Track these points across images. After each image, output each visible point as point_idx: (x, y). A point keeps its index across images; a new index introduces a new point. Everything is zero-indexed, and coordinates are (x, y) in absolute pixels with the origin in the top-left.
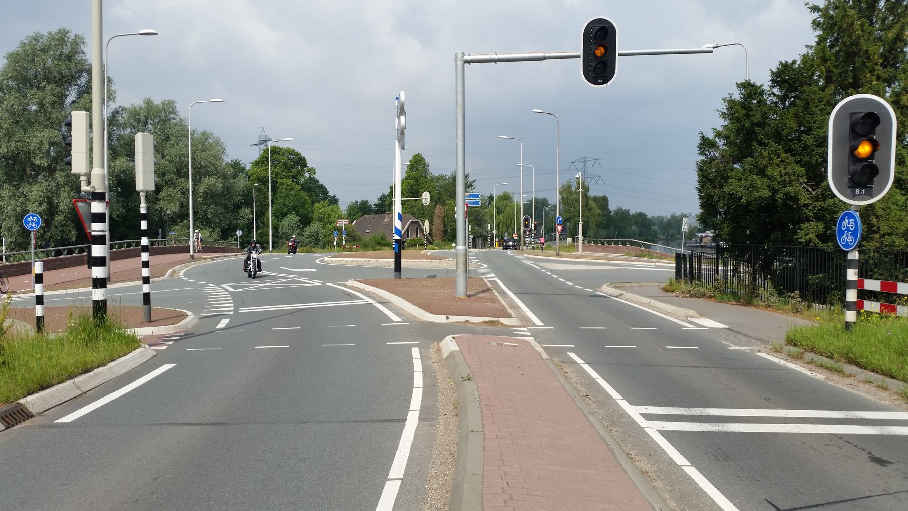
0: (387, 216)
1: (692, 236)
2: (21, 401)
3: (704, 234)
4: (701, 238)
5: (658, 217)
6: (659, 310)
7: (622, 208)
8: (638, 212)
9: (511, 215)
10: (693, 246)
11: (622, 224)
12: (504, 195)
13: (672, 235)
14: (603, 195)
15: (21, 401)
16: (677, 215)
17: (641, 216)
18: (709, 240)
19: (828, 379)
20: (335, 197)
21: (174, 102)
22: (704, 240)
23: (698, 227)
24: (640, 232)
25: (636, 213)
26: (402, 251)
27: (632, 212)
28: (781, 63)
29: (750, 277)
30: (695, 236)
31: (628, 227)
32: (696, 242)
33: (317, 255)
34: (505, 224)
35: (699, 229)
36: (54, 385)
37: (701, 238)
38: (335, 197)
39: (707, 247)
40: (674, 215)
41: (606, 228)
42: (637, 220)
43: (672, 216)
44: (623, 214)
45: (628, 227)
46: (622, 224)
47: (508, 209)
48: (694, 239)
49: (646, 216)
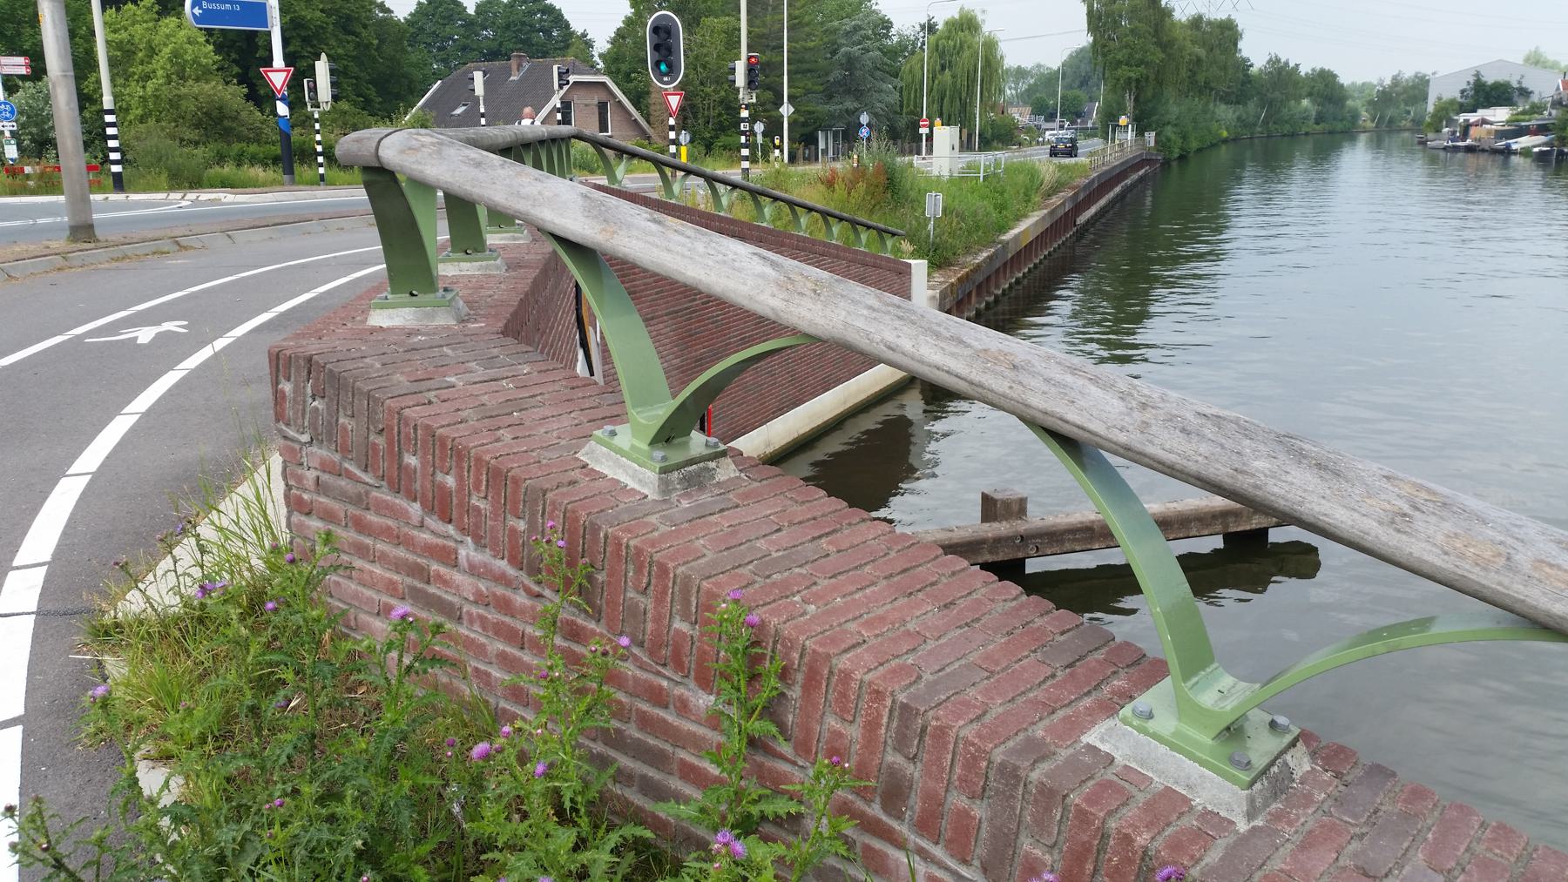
0: (514, 67)
1: (1441, 121)
3: (1473, 118)
4: (1466, 128)
6: (1178, 474)
7: (1280, 56)
8: (1318, 68)
10: (1445, 149)
11: (1277, 94)
12: (961, 18)
13: (1391, 121)
18: (1489, 132)
20: (584, 35)
21: (1417, 73)
22: (1473, 131)
23: (1459, 100)
24: (1319, 113)
25: (1313, 70)
27: (1304, 70)
29: (1199, 220)
30: (1450, 122)
33: (18, 223)
34: (957, 95)
35: (1461, 105)
36: (1530, 620)
37: (1466, 128)
38: (584, 35)
39: (1483, 151)
40: (1399, 75)
41: (1238, 103)
43: (1395, 78)
46: (1277, 94)
47: (966, 54)
48: (1446, 130)
49: (1335, 76)
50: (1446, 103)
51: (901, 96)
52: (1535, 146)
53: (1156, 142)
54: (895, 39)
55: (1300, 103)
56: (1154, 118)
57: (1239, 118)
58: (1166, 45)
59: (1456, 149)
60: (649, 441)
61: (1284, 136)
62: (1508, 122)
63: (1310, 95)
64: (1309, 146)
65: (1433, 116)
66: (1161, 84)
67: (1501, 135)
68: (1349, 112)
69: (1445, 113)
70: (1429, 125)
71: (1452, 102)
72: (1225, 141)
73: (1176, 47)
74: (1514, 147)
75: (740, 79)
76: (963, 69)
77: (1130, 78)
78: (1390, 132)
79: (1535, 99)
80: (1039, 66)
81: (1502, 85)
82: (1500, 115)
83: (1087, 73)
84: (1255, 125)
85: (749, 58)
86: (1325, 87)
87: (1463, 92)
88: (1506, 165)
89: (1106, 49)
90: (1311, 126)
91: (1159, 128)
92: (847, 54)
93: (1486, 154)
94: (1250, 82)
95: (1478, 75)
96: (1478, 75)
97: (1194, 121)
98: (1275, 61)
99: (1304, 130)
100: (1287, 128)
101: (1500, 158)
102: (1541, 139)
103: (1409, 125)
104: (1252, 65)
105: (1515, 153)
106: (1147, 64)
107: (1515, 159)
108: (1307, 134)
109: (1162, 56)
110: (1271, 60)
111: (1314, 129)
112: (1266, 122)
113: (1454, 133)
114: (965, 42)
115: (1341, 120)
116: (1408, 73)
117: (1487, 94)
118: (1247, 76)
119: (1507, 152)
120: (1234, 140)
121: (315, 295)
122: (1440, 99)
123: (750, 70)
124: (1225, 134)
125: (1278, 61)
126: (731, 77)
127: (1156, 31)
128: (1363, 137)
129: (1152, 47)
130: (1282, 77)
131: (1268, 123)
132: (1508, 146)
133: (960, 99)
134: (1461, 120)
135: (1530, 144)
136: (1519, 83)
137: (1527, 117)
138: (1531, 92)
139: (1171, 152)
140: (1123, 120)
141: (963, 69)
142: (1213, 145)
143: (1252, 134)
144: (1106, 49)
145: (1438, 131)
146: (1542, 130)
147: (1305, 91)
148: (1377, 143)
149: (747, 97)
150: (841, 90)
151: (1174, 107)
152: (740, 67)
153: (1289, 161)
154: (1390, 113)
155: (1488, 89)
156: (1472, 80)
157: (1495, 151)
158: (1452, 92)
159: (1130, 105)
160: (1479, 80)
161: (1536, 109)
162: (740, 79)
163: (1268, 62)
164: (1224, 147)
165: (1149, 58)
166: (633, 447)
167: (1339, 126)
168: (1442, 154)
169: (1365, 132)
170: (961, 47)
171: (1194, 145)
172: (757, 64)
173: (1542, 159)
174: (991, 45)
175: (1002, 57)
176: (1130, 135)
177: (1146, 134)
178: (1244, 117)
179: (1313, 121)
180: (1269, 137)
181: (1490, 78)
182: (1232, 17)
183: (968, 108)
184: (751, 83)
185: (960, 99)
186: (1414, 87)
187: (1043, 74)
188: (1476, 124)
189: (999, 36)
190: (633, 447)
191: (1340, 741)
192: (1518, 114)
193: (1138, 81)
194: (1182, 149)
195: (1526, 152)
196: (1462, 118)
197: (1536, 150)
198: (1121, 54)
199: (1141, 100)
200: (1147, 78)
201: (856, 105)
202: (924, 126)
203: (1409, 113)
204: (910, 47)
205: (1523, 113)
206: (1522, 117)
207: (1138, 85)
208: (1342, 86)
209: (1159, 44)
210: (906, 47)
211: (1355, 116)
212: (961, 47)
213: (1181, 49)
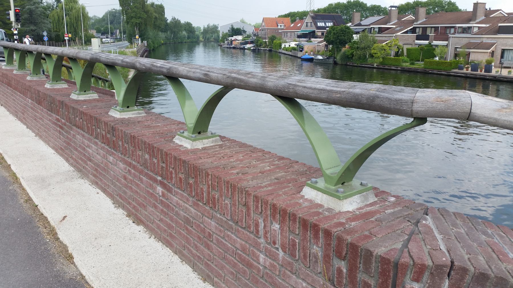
1: (224, 40)
2: (146, 115)
4: (232, 41)
5: (197, 27)
7: (175, 17)
8: (186, 22)
9: (77, 18)
13: (208, 39)
14: (160, 4)
15: (146, 115)
16: (211, 25)
17: (189, 25)
18: (238, 43)
19: (78, 97)
26: (300, 60)
28: (455, 2)
30: (227, 40)
31: (180, 32)
32: (228, 44)
40: (209, 25)
41: (165, 32)
42: (186, 28)
43: (208, 25)
44: (176, 22)
45: (180, 32)
46: (176, 29)
47: (74, 11)
48: (226, 42)
49: (191, 24)
50: (225, 34)
51: (53, 25)
52: (252, 47)
53: (147, 44)
54: (45, 4)
55: (182, 33)
56: (145, 36)
57: (166, 37)
58: (147, 12)
59: (230, 48)
60: (192, 133)
61: (179, 43)
62: (243, 40)
63: (185, 30)
64: (186, 46)
65: (222, 38)
66: (146, 25)
67: (242, 44)
68: (196, 36)
69: (225, 37)
70: (221, 40)
71: (227, 33)
72: (163, 44)
73: (150, 13)
74: (246, 47)
75: (12, 18)
76: (73, 16)
77: (136, 23)
78: (208, 42)
79: (248, 33)
80: (95, 16)
81: (239, 29)
82: (240, 38)
83: (112, 19)
84: (170, 39)
85: (15, 10)
86: (188, 27)
87: (229, 31)
88: (244, 54)
89: (127, 12)
90: (186, 40)
91: (147, 39)
92: (29, 9)
93: (238, 49)
94: (168, 25)
95: (232, 26)
96: (232, 26)
97: (155, 37)
98: (174, 19)
99: (185, 41)
100: (180, 40)
101: (242, 51)
102: (251, 45)
103: (213, 40)
104: (168, 20)
105: (246, 49)
106: (141, 18)
107: (246, 51)
108: (185, 42)
109: (146, 16)
110: (173, 18)
111: (187, 41)
112: (173, 38)
113: (228, 43)
114: (73, 7)
115: (195, 38)
116: (211, 24)
117: (235, 32)
118: (167, 23)
119: (244, 49)
120: (165, 44)
121: (61, 87)
122: (223, 33)
123: (17, 15)
124: (163, 42)
125: (175, 19)
126: (8, 17)
127: (143, 7)
128: (201, 44)
129: (143, 13)
130: (176, 23)
131: (174, 39)
132: (244, 47)
133: (74, 27)
134: (230, 39)
135: (250, 47)
136: (243, 28)
137: (247, 39)
138: (246, 31)
139: (151, 48)
140: (137, 37)
141: (73, 16)
142: (160, 45)
143: (170, 42)
144: (127, 12)
145: (224, 42)
146: (252, 42)
147: (183, 29)
148: (205, 46)
149: (16, 25)
150: (28, 22)
151: (151, 33)
152: (12, 13)
153: (181, 52)
154: (208, 36)
155: (235, 30)
156: (231, 27)
157: (241, 49)
158: (226, 31)
159: (137, 32)
160: (232, 27)
161: (249, 36)
162: (12, 18)
163: (172, 19)
164: (163, 46)
165: (142, 16)
166: (189, 135)
167: (194, 40)
168: (226, 49)
169: (201, 42)
170: (72, 8)
171: (156, 45)
172: (19, 12)
173: (254, 51)
174: (83, 8)
175: (87, 13)
176: (140, 42)
177: (144, 42)
178: (167, 37)
179: (186, 39)
180: (175, 43)
181: (235, 27)
182: (162, 4)
183: (77, 30)
184: (17, 20)
185: (74, 27)
186: (213, 29)
187: (97, 19)
188: (234, 40)
189: (85, 5)
190: (189, 135)
191: (75, 255)
192: (244, 38)
193: (139, 24)
194: (154, 47)
195: (249, 49)
196: (230, 38)
197: (252, 48)
198: (133, 14)
199: (140, 30)
200: (142, 23)
201: (35, 28)
202: (66, 36)
203: (212, 36)
204: (51, 7)
205: (246, 37)
206: (246, 39)
207: (139, 25)
208: (194, 27)
209: (144, 12)
210: (50, 7)
211: (198, 37)
212: (72, 8)
213: (151, 14)
